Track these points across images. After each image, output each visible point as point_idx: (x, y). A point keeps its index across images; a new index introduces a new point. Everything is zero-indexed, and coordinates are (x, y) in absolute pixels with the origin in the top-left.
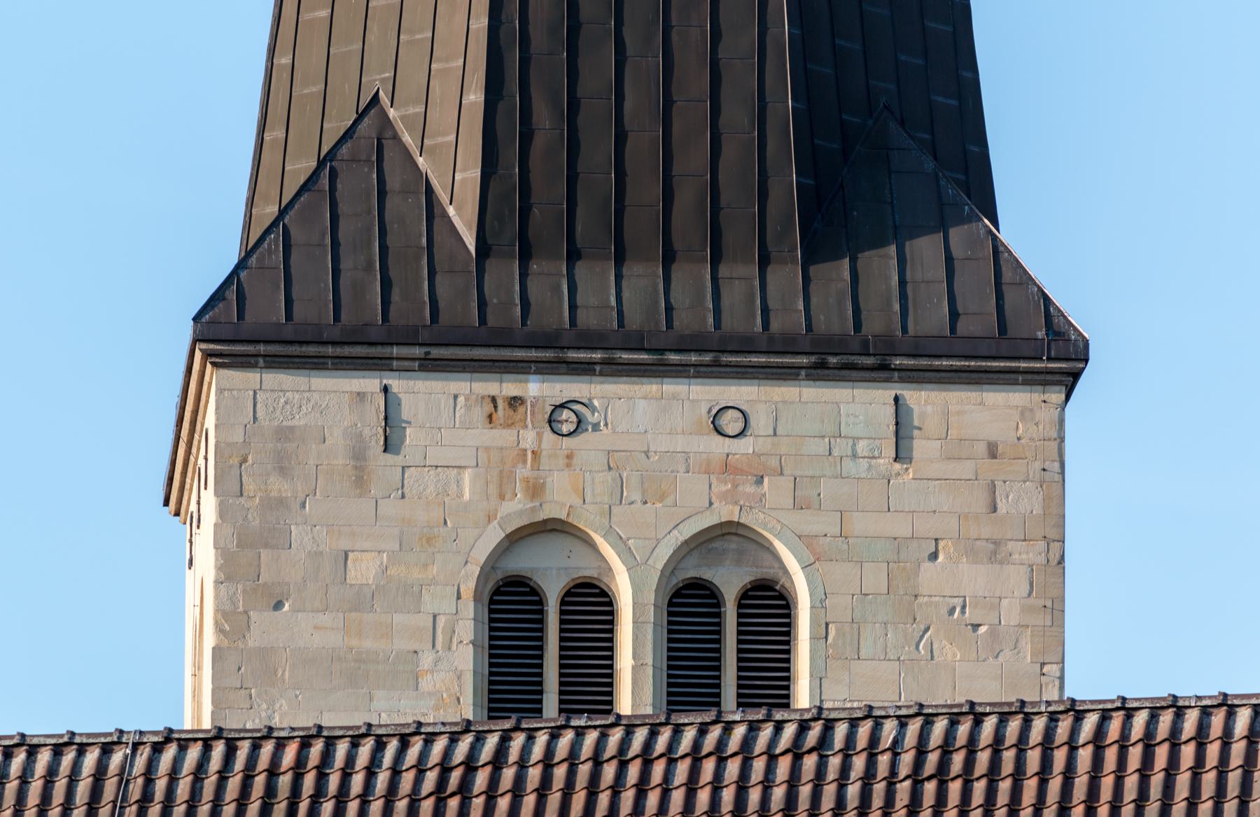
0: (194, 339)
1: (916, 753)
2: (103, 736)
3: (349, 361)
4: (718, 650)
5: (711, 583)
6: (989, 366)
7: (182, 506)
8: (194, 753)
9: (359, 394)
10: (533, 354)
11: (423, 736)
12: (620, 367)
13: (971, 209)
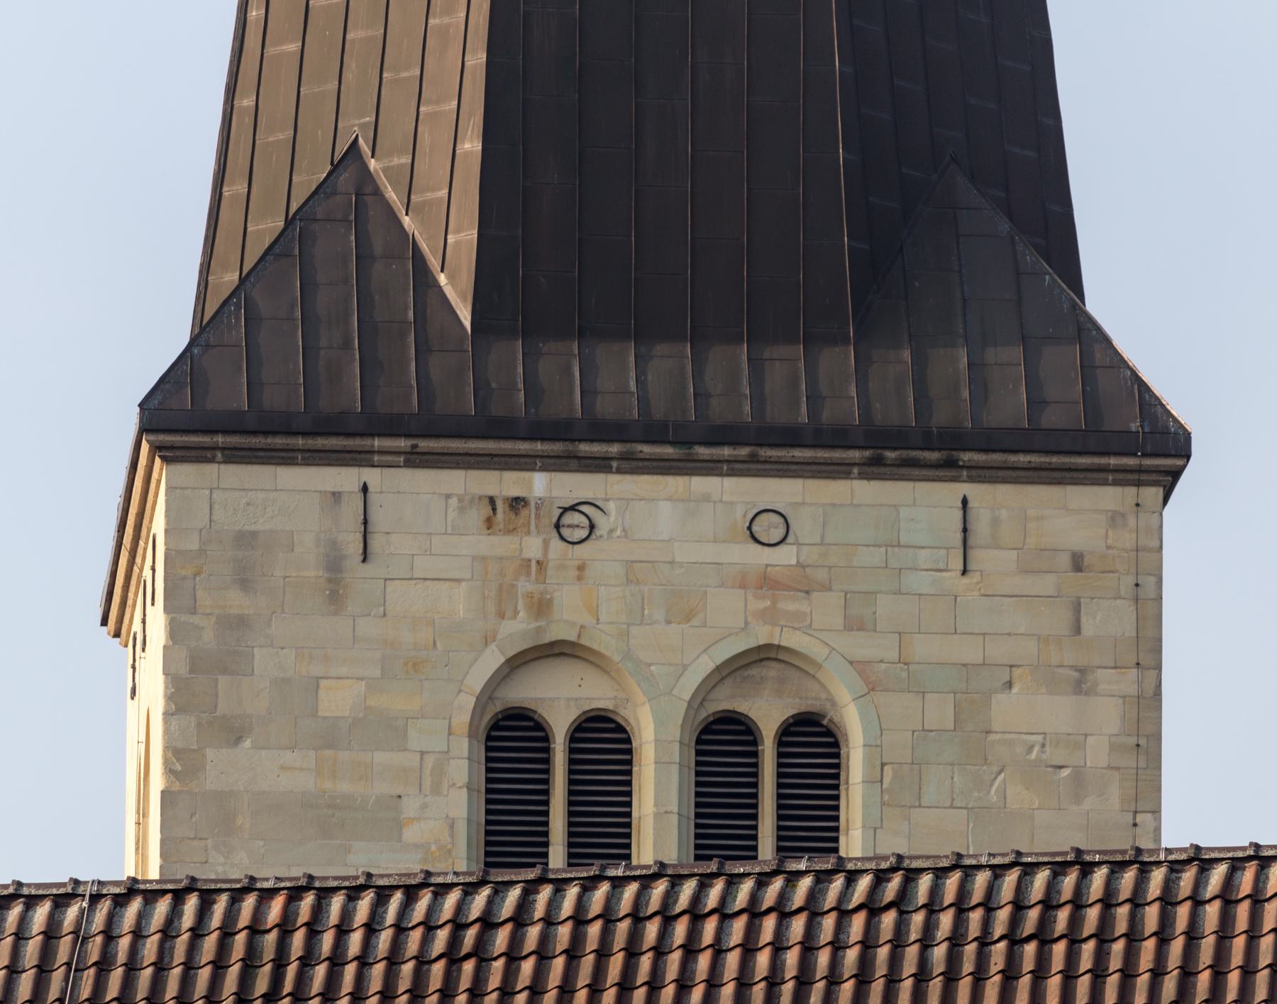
0: (140, 428)
1: (1013, 909)
2: (55, 887)
3: (322, 455)
4: (755, 796)
5: (746, 716)
6: (1073, 463)
7: (124, 625)
8: (162, 907)
9: (334, 494)
10: (539, 446)
11: (431, 888)
12: (641, 464)
13: (1053, 280)
